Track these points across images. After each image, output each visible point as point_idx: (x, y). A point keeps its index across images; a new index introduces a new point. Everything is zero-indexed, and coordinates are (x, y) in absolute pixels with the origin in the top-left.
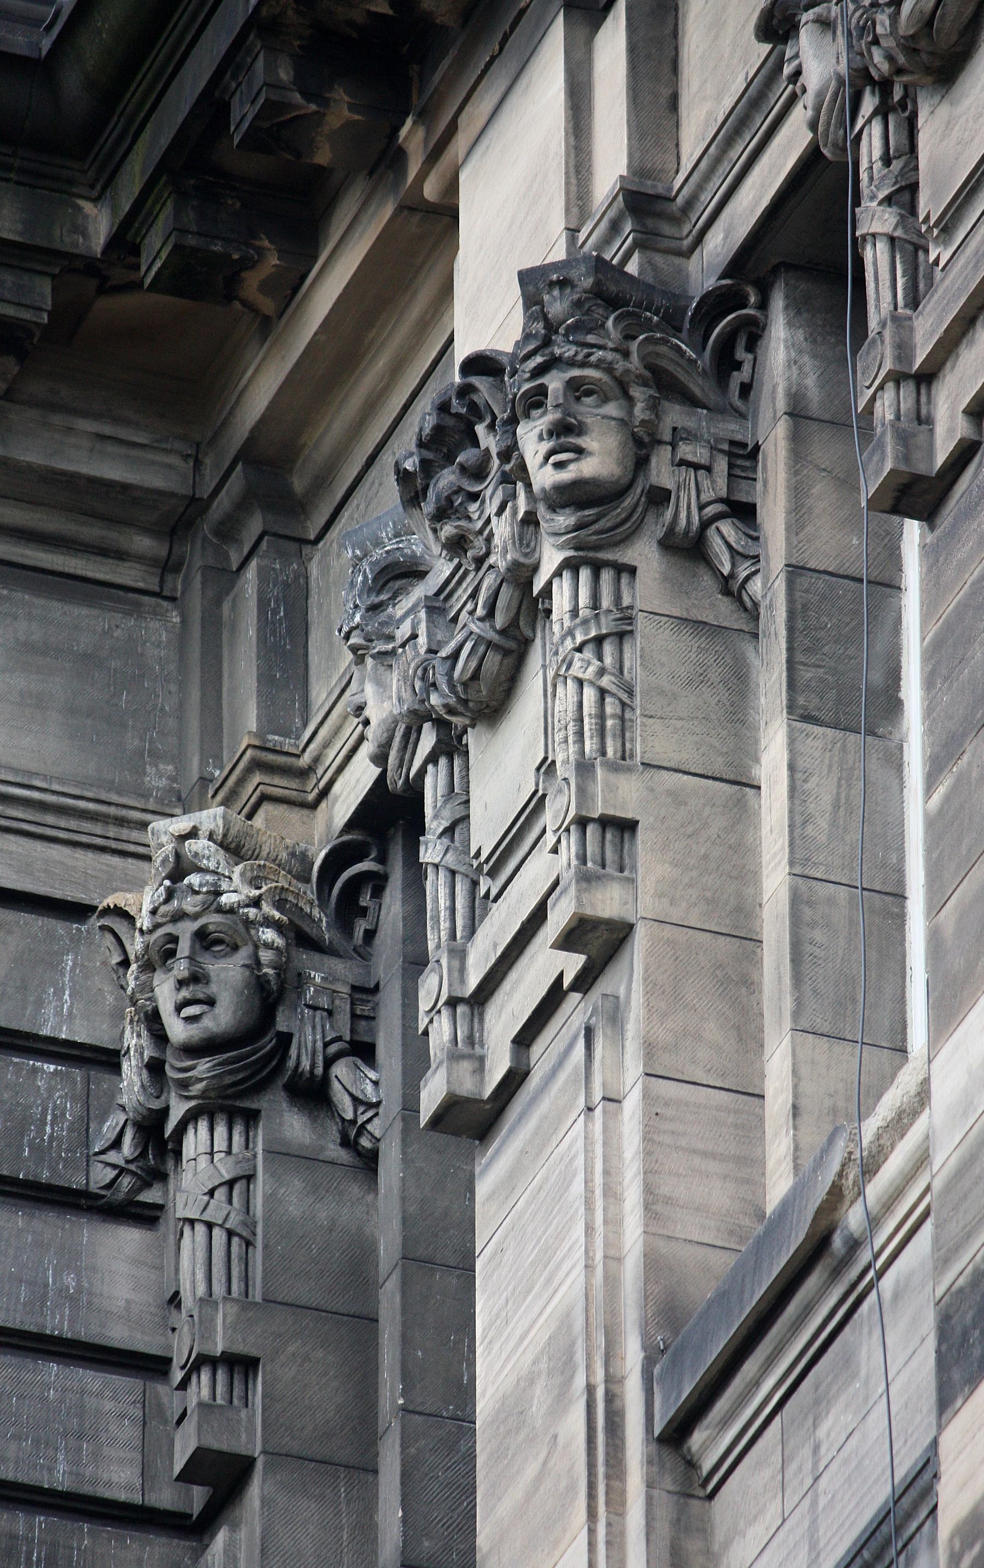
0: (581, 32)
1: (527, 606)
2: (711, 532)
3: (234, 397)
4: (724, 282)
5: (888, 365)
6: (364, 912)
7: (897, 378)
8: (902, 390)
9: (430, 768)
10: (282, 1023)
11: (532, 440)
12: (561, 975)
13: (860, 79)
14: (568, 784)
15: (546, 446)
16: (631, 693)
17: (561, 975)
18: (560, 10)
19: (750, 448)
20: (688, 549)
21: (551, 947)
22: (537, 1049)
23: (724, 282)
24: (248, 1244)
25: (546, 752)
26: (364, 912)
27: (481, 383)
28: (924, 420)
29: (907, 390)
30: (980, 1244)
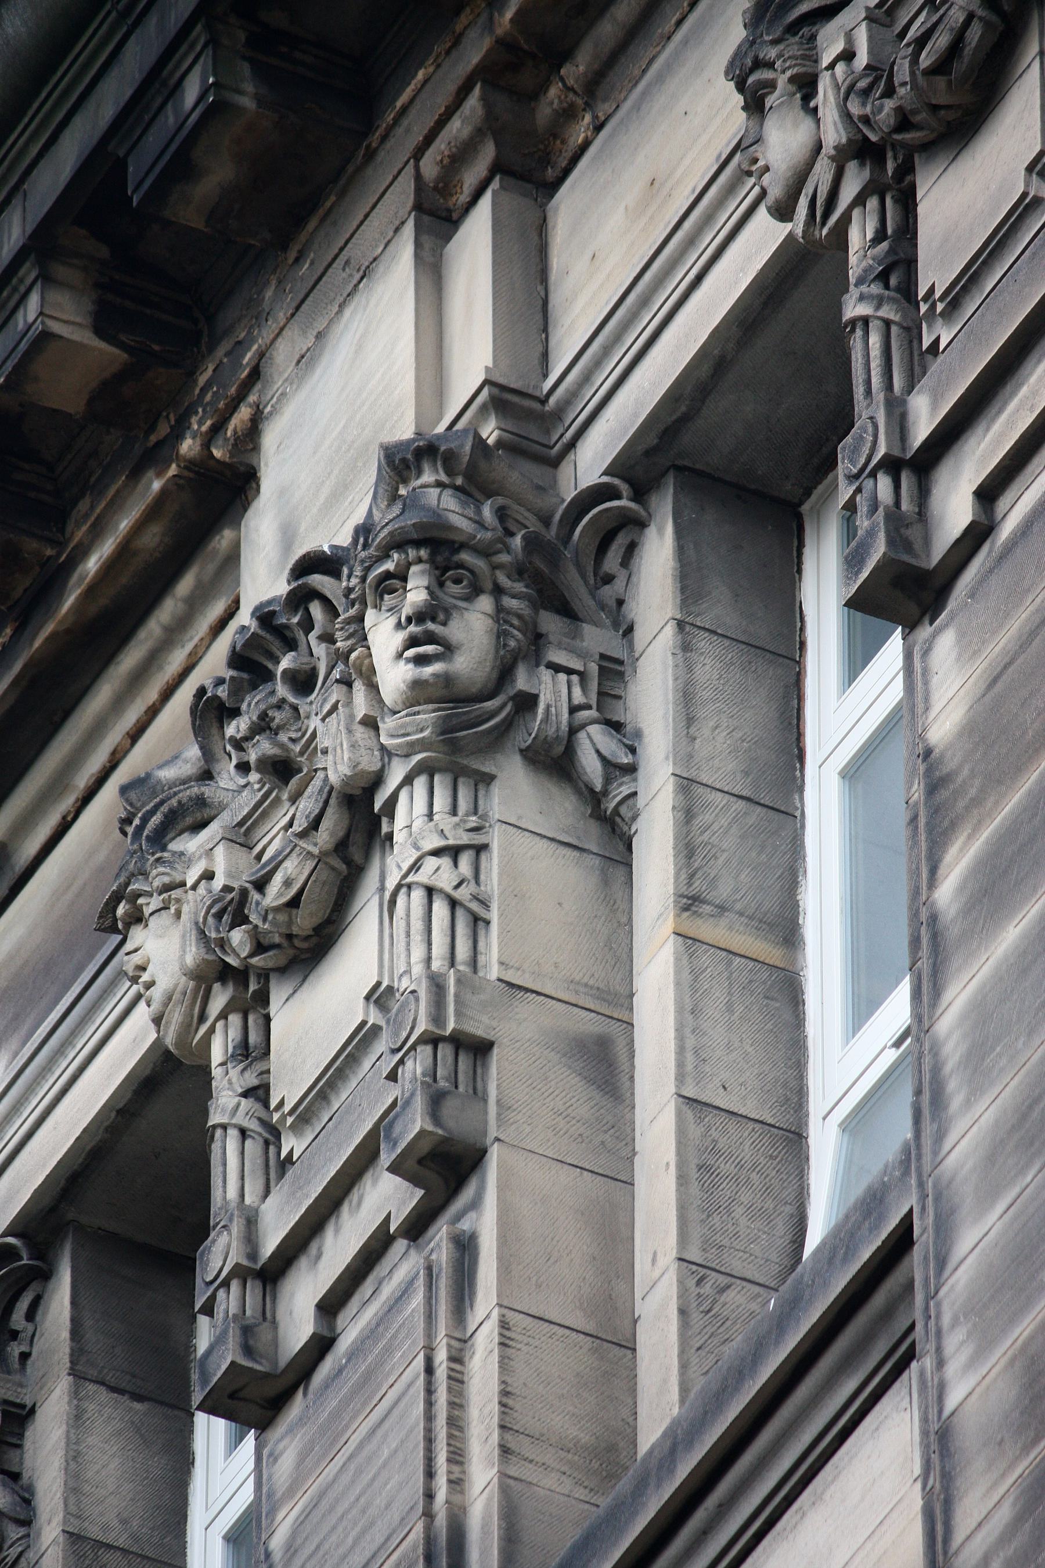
0: (427, 241)
1: (361, 819)
2: (582, 735)
3: (390, 117)
4: (10, 1240)
5: (882, 451)
6: (14, 1335)
7: (892, 465)
8: (248, 1285)
9: (856, 213)
10: (522, 682)
11: (384, 636)
12: (387, 1219)
13: (214, 972)
14: (417, 1000)
15: (400, 637)
16: (485, 904)
17: (387, 1219)
18: (410, 214)
19: (27, 1409)
20: (555, 761)
21: (387, 1169)
22: (1002, 504)
23: (10, 1240)
24: (477, 922)
25: (381, 973)
26: (14, 1335)
27: (318, 581)
28: (268, 1316)
29: (254, 1289)
30: (1042, 1305)
